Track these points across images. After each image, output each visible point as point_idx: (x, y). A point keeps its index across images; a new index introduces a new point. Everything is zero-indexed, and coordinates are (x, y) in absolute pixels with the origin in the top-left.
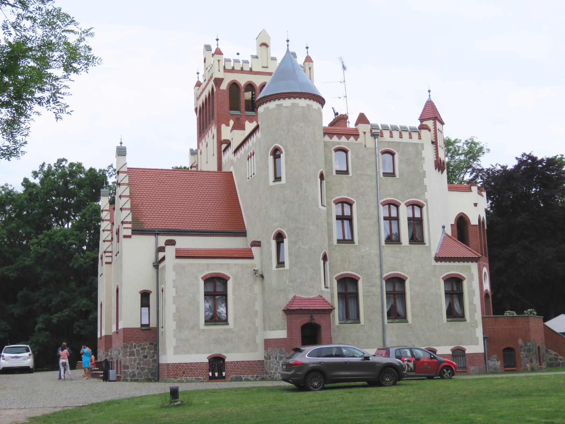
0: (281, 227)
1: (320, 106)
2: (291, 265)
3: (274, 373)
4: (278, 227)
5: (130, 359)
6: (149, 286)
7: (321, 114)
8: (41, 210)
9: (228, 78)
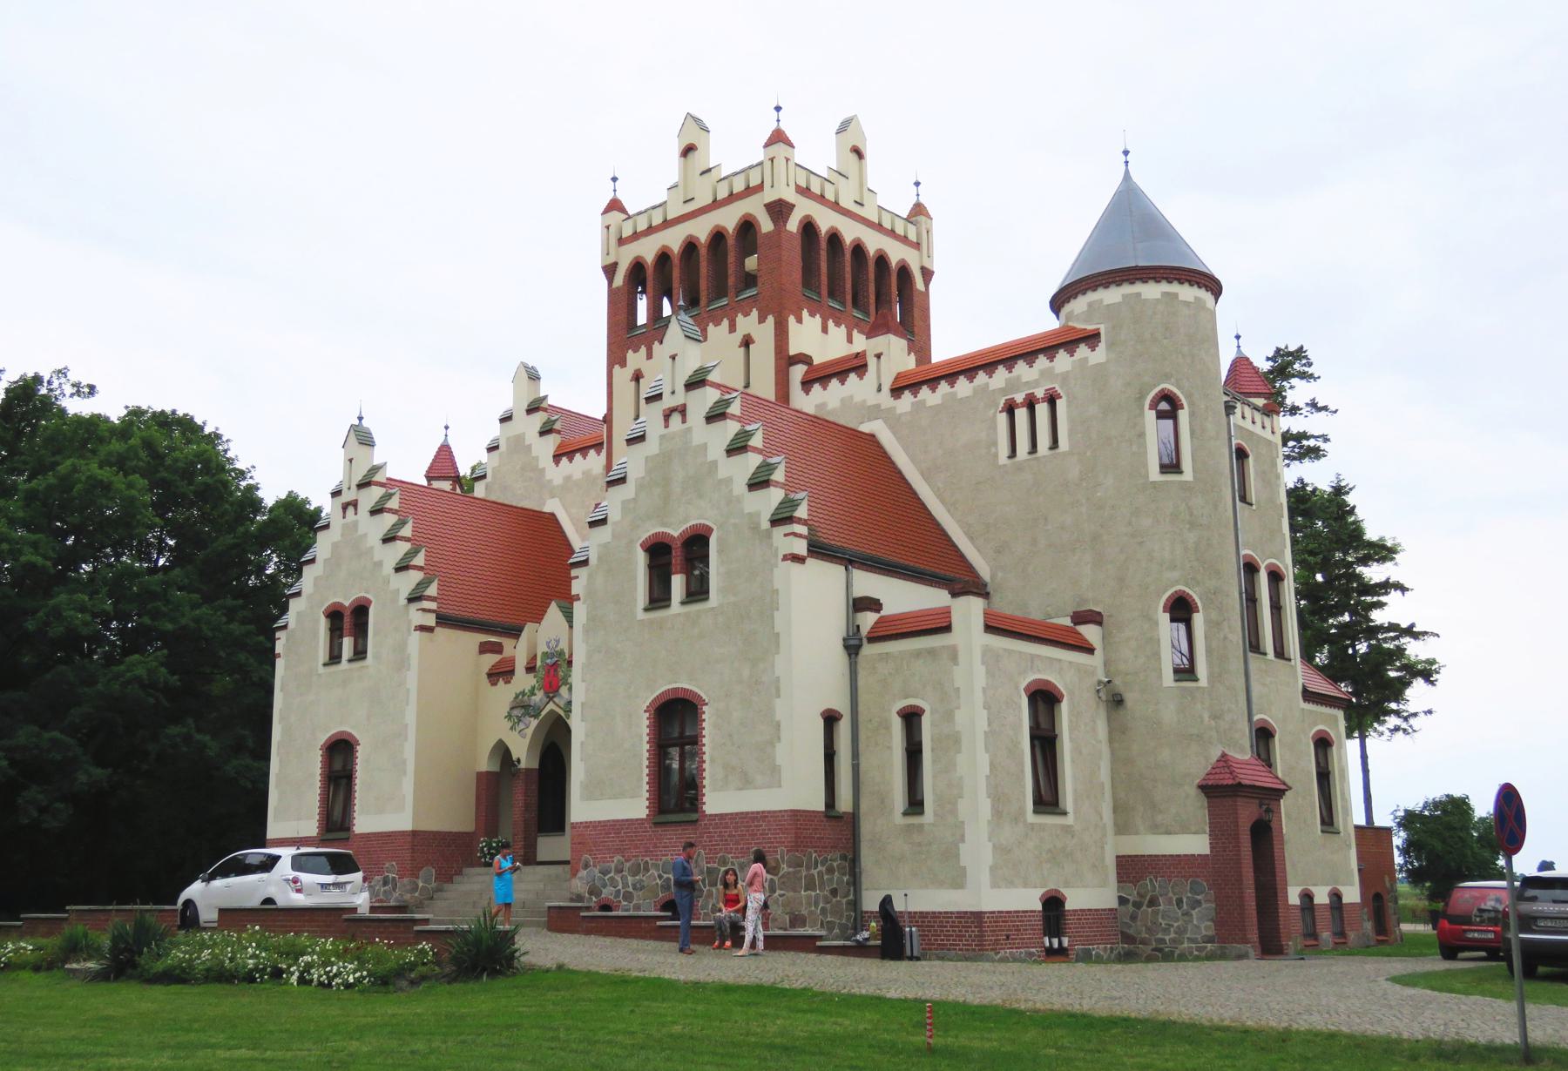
0: (1187, 585)
1: (1207, 297)
2: (1212, 678)
3: (1173, 941)
4: (1177, 582)
5: (809, 897)
6: (841, 705)
7: (1213, 314)
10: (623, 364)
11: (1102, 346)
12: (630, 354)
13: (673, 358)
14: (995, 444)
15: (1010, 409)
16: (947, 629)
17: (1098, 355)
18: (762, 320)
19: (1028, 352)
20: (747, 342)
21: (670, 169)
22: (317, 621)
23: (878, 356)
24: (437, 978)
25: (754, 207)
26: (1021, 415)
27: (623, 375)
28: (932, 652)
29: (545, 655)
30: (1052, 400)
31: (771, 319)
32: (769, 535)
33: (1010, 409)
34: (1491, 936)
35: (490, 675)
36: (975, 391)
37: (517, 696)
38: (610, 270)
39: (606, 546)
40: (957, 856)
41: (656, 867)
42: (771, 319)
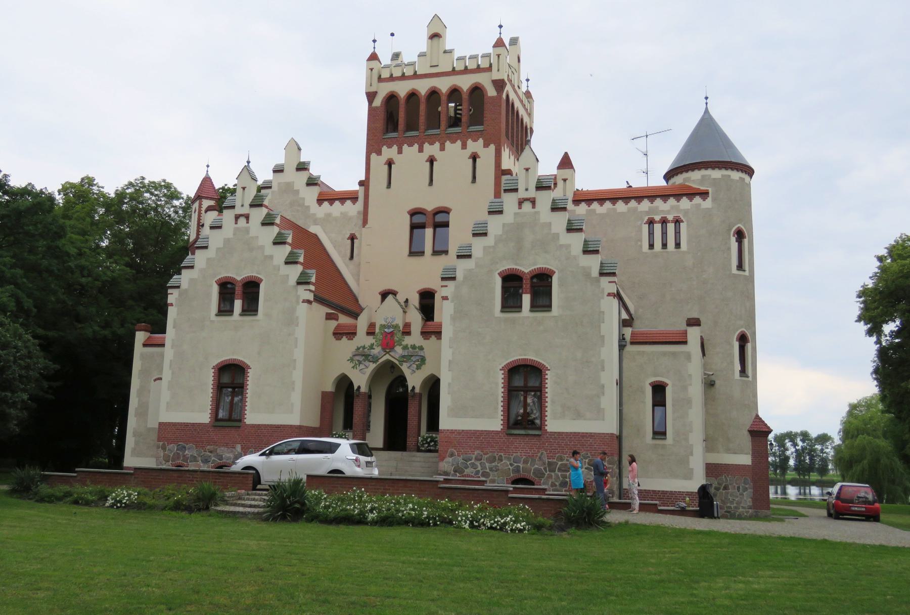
3: (736, 508)
4: (742, 327)
8: (44, 249)
9: (384, 90)
10: (379, 153)
11: (709, 200)
12: (384, 148)
13: (527, 170)
14: (641, 240)
15: (651, 222)
16: (685, 343)
17: (708, 204)
18: (486, 145)
19: (651, 195)
20: (474, 157)
21: (423, 44)
22: (211, 286)
23: (565, 180)
24: (551, 528)
25: (484, 80)
26: (658, 228)
27: (378, 162)
28: (674, 354)
29: (383, 326)
30: (677, 222)
31: (492, 147)
32: (599, 281)
33: (651, 222)
34: (864, 509)
35: (335, 334)
36: (629, 209)
37: (358, 349)
38: (371, 96)
39: (470, 270)
40: (688, 462)
41: (509, 459)
42: (492, 147)
